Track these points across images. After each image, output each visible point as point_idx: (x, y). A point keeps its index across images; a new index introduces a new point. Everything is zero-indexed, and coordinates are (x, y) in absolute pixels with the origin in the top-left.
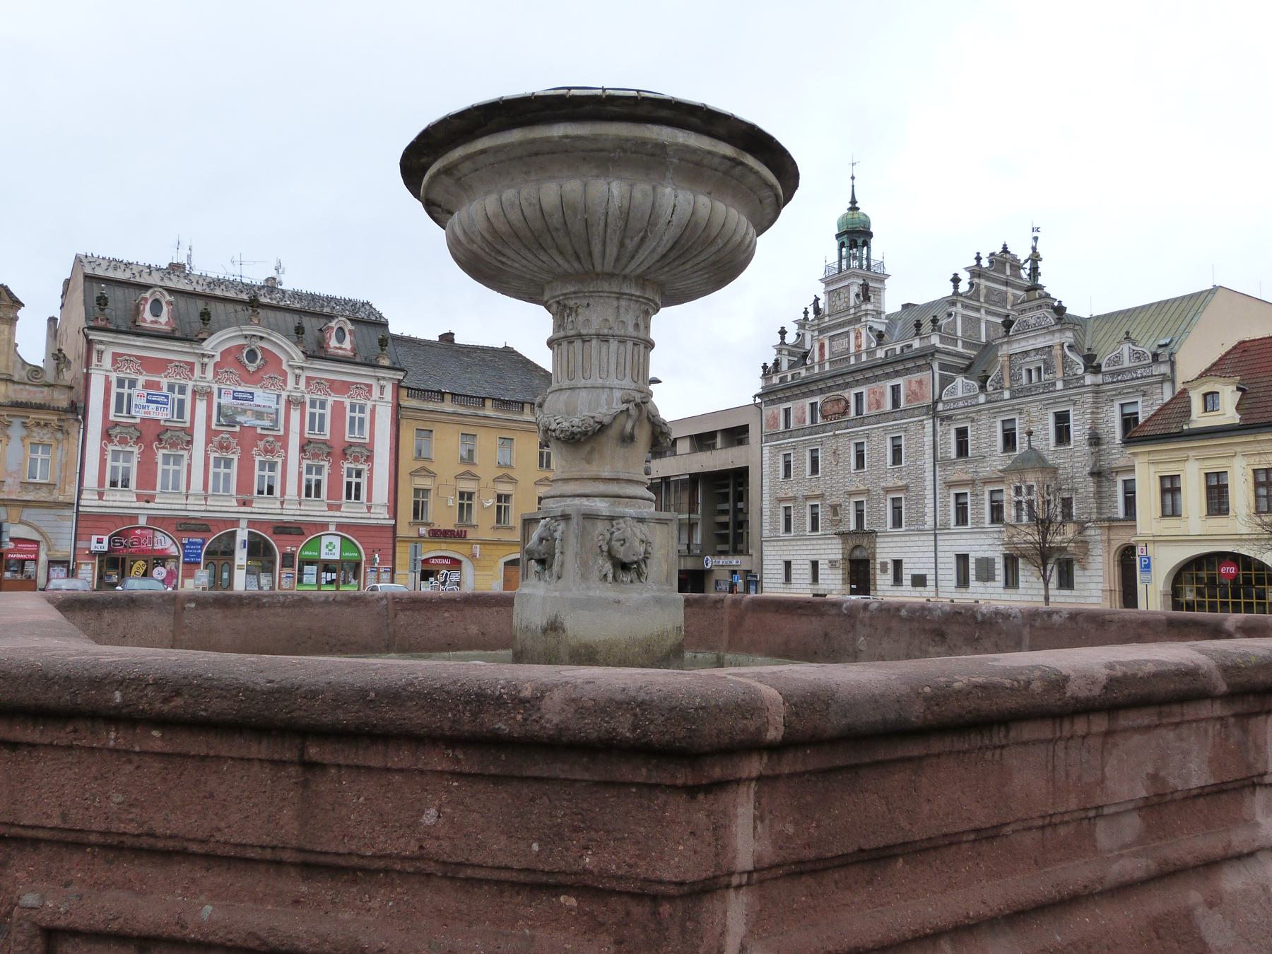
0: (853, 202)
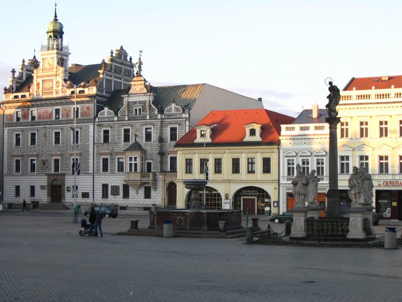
0: (56, 16)
